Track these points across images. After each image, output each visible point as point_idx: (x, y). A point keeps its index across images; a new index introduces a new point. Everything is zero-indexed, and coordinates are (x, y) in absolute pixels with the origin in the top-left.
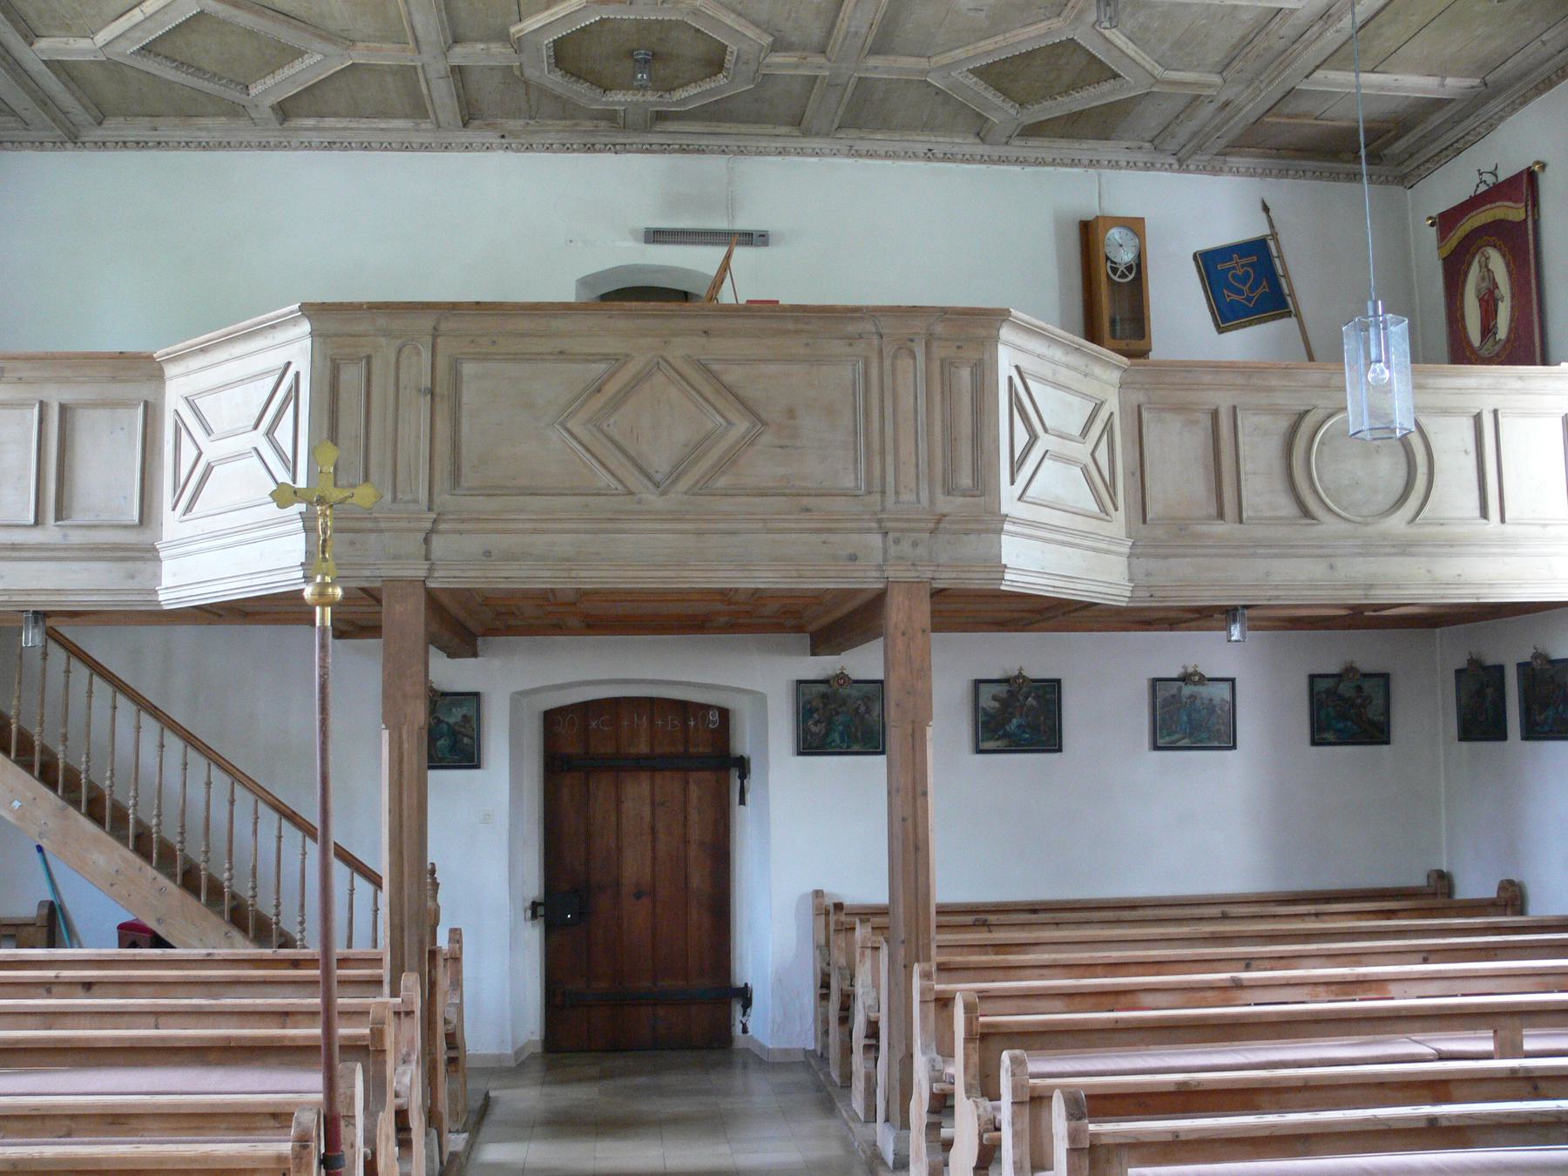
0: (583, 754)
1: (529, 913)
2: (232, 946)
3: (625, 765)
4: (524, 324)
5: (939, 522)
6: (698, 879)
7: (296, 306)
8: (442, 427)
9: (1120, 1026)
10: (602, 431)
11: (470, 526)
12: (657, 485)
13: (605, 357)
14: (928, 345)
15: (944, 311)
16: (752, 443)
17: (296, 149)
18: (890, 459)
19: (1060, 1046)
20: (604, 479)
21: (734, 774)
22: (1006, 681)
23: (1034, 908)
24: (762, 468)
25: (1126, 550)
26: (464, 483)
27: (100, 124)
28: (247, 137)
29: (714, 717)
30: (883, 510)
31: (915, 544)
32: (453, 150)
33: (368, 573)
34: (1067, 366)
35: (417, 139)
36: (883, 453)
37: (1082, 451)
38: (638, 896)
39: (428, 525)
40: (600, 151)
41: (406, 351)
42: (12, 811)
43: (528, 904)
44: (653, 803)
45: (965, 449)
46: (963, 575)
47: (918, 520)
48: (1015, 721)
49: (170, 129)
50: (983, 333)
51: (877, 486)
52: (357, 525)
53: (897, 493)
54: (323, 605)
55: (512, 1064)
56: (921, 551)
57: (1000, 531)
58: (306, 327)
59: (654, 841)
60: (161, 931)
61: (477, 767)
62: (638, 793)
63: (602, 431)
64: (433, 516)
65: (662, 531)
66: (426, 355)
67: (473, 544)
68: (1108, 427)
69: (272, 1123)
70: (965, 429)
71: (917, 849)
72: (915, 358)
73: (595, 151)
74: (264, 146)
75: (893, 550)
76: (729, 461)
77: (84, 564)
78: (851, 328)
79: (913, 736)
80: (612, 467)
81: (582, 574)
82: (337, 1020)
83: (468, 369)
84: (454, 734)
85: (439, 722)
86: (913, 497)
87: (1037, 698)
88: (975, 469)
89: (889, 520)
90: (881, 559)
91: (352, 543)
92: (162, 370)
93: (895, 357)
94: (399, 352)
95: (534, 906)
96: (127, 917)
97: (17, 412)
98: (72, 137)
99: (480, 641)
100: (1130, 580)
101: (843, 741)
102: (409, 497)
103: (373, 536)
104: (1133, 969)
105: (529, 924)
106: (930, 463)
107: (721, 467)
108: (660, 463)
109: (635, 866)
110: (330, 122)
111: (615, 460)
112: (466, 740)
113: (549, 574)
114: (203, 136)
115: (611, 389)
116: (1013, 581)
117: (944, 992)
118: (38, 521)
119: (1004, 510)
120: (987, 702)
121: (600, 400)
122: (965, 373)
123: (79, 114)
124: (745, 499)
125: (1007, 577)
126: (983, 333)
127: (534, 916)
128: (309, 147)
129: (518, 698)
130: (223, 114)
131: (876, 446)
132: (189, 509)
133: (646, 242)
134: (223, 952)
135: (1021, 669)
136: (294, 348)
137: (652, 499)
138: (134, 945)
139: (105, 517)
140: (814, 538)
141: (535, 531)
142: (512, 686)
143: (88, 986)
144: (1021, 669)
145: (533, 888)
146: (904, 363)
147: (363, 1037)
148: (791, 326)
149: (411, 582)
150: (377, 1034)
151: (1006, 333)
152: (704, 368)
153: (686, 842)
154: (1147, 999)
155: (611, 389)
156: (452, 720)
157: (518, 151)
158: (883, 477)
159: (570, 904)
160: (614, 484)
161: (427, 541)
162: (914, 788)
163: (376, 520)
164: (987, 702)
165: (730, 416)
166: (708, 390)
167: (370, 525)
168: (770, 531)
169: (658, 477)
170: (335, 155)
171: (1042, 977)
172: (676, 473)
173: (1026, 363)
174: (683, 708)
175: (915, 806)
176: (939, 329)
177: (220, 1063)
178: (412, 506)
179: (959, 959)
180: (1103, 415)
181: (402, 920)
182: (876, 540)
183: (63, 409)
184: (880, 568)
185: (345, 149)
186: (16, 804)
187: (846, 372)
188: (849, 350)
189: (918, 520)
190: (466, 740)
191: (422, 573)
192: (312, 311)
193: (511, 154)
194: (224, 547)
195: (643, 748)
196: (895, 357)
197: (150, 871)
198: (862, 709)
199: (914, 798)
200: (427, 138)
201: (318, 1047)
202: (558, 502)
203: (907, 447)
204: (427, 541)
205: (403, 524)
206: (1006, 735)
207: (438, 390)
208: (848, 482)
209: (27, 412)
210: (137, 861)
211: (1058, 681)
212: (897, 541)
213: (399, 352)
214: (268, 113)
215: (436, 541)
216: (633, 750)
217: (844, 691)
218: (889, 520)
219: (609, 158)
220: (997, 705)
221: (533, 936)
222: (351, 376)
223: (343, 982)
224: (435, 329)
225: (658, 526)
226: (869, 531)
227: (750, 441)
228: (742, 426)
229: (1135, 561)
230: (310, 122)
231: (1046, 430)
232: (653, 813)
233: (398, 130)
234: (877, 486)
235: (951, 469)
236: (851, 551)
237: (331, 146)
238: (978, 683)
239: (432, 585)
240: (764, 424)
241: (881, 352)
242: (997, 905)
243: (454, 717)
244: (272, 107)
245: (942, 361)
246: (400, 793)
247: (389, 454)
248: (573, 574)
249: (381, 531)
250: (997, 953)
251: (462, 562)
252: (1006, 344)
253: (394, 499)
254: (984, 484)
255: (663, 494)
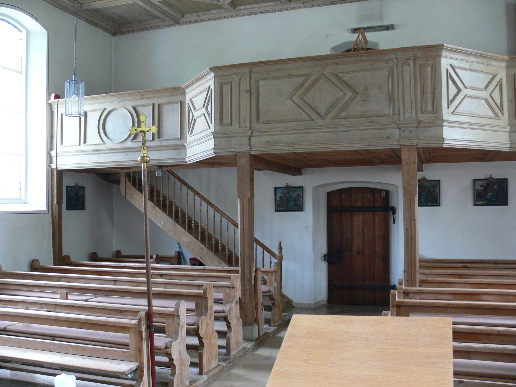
0: (340, 207)
1: (323, 258)
2: (221, 266)
3: (354, 210)
4: (278, 67)
5: (419, 124)
6: (378, 248)
7: (208, 69)
8: (254, 102)
9: (449, 306)
10: (303, 100)
11: (263, 134)
12: (321, 117)
13: (303, 75)
14: (414, 61)
15: (418, 48)
16: (353, 100)
17: (241, 16)
18: (401, 103)
19: (430, 312)
20: (304, 116)
21: (391, 213)
22: (486, 179)
23: (496, 262)
24: (357, 108)
25: (508, 130)
26: (261, 120)
27: (183, 17)
28: (225, 15)
29: (383, 193)
30: (399, 120)
31: (410, 132)
32: (289, 10)
33: (232, 150)
34: (477, 62)
35: (277, 8)
36: (398, 100)
37: (485, 94)
38: (358, 253)
39: (249, 134)
40: (336, 4)
41: (242, 79)
42: (161, 224)
43: (323, 255)
44: (363, 223)
45: (429, 97)
46: (428, 142)
47: (411, 123)
48: (489, 194)
49: (203, 15)
50: (435, 54)
51: (397, 112)
52: (228, 135)
53: (404, 114)
54: (144, 163)
55: (314, 307)
56: (413, 134)
57: (442, 126)
58: (212, 74)
59: (364, 235)
60: (202, 261)
61: (302, 211)
62: (358, 219)
63: (303, 100)
64: (250, 131)
65: (321, 132)
66: (248, 80)
67: (264, 139)
68: (500, 83)
69: (159, 316)
70: (429, 90)
71: (412, 239)
72: (410, 65)
73: (334, 4)
74: (231, 17)
75: (402, 134)
76: (346, 106)
77: (166, 151)
78: (387, 57)
79: (410, 199)
80: (307, 112)
81: (297, 147)
82: (151, 285)
83: (261, 83)
84: (295, 200)
85: (290, 196)
86: (409, 115)
87: (498, 185)
88: (433, 104)
89: (400, 124)
90: (398, 138)
91: (228, 141)
92: (185, 91)
93: (402, 66)
94: (240, 80)
95: (325, 256)
96: (193, 257)
97: (147, 107)
98: (177, 22)
99: (302, 170)
100: (510, 141)
101: (425, 201)
102: (244, 125)
103: (234, 138)
104: (498, 286)
105: (323, 262)
106: (416, 103)
107: (342, 110)
108: (322, 110)
109: (357, 244)
110: (249, 6)
111: (308, 109)
112: (299, 202)
113: (287, 148)
114: (213, 16)
115: (306, 85)
116: (447, 143)
117: (406, 290)
118: (153, 139)
119: (444, 118)
120: (478, 187)
121: (302, 90)
122: (429, 69)
123: (177, 16)
124: (350, 119)
125: (445, 142)
126: (435, 54)
127: (325, 259)
128: (244, 15)
129: (316, 189)
130: (217, 9)
131: (396, 99)
132: (192, 133)
133: (352, 33)
134: (220, 268)
135: (491, 175)
136: (210, 81)
137: (320, 121)
138: (194, 265)
139: (171, 137)
140: (375, 131)
141: (283, 134)
142: (314, 184)
143: (161, 275)
144: (491, 175)
145: (324, 249)
146: (406, 68)
147: (201, 293)
148: (365, 58)
149: (245, 152)
150: (205, 292)
151: (444, 53)
152: (336, 76)
153: (375, 236)
154: (485, 297)
155: (306, 85)
156: (294, 196)
157: (309, 7)
158: (399, 109)
159: (336, 256)
160: (308, 117)
161: (250, 139)
162: (411, 218)
163: (234, 133)
164: (478, 187)
165: (345, 92)
166: (338, 83)
167: (232, 135)
168: (360, 130)
169: (322, 114)
170: (253, 16)
171: (462, 287)
172: (328, 113)
173: (455, 63)
174: (373, 191)
175: (411, 224)
176: (419, 54)
177: (165, 298)
178: (245, 129)
179: (431, 279)
180: (497, 79)
181: (244, 258)
182: (397, 131)
183: (159, 105)
184: (398, 141)
185: (255, 14)
186: (162, 222)
187: (385, 73)
188: (386, 65)
189: (411, 123)
190: (299, 202)
191: (248, 150)
192: (213, 69)
193: (307, 9)
194: (198, 144)
195: (359, 204)
196: (402, 66)
197: (199, 243)
198: (432, 190)
199: (411, 222)
200: (280, 7)
201: (146, 293)
202: (289, 124)
203: (407, 97)
204: (250, 139)
205: (242, 134)
206: (486, 199)
207: (252, 91)
208: (387, 111)
209: (175, 105)
210: (195, 240)
211: (506, 179)
212: (404, 131)
213: (240, 80)
214: (229, 7)
215: (253, 139)
216: (356, 205)
217: (425, 184)
218: (400, 124)
219: (339, 6)
220: (482, 188)
221: (324, 266)
222: (226, 88)
223: (152, 274)
224: (250, 71)
225: (322, 130)
226: (394, 128)
227: (352, 99)
228: (349, 94)
229: (512, 134)
230: (243, 7)
231: (465, 87)
232: (363, 226)
233: (270, 6)
234: (397, 112)
235: (424, 103)
236: (388, 136)
237: (251, 14)
238: (475, 180)
239: (252, 153)
240: (357, 93)
241: (397, 64)
242: (480, 260)
243: (295, 195)
244: (229, 4)
245: (420, 66)
246: (243, 219)
247: (238, 112)
248: (295, 148)
249: (236, 137)
250: (459, 278)
251: (261, 145)
252: (445, 57)
253: (240, 126)
254: (437, 109)
255: (323, 119)
